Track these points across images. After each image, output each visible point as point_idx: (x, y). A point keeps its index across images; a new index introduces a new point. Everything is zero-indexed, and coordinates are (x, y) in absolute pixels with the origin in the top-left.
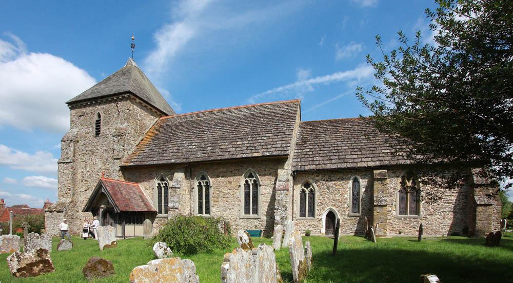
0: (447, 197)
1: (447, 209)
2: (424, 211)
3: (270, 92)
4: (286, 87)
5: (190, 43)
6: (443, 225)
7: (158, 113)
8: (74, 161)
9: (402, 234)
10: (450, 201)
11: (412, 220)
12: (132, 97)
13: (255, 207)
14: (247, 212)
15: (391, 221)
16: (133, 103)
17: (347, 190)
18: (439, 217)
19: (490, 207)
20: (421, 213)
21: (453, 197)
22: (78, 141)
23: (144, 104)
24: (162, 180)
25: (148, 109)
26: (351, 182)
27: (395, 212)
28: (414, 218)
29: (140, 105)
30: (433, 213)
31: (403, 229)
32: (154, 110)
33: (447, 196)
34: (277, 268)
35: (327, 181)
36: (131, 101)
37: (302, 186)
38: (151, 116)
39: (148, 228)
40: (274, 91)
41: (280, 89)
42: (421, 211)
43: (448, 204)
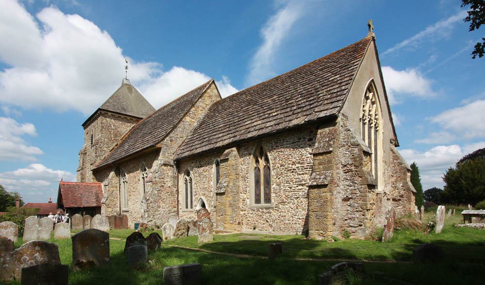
0: (300, 176)
1: (300, 193)
2: (276, 198)
3: (390, 50)
4: (413, 38)
5: (296, 25)
6: (296, 217)
7: (134, 119)
8: (82, 169)
9: (257, 230)
10: (303, 182)
11: (264, 210)
12: (103, 112)
13: (258, 192)
14: (258, 201)
15: (246, 212)
16: (105, 117)
17: (212, 175)
18: (292, 206)
19: (325, 189)
20: (273, 201)
21: (306, 176)
22: (86, 153)
23: (117, 115)
24: (188, 175)
25: (122, 119)
26: (214, 166)
27: (250, 200)
28: (266, 208)
29: (116, 118)
30: (285, 200)
31: (257, 223)
32: (129, 118)
33: (300, 174)
34: (41, 257)
35: (198, 167)
36: (102, 116)
37: (184, 174)
38: (126, 124)
39: (77, 221)
40: (396, 48)
41: (405, 43)
42: (272, 198)
43: (301, 187)
